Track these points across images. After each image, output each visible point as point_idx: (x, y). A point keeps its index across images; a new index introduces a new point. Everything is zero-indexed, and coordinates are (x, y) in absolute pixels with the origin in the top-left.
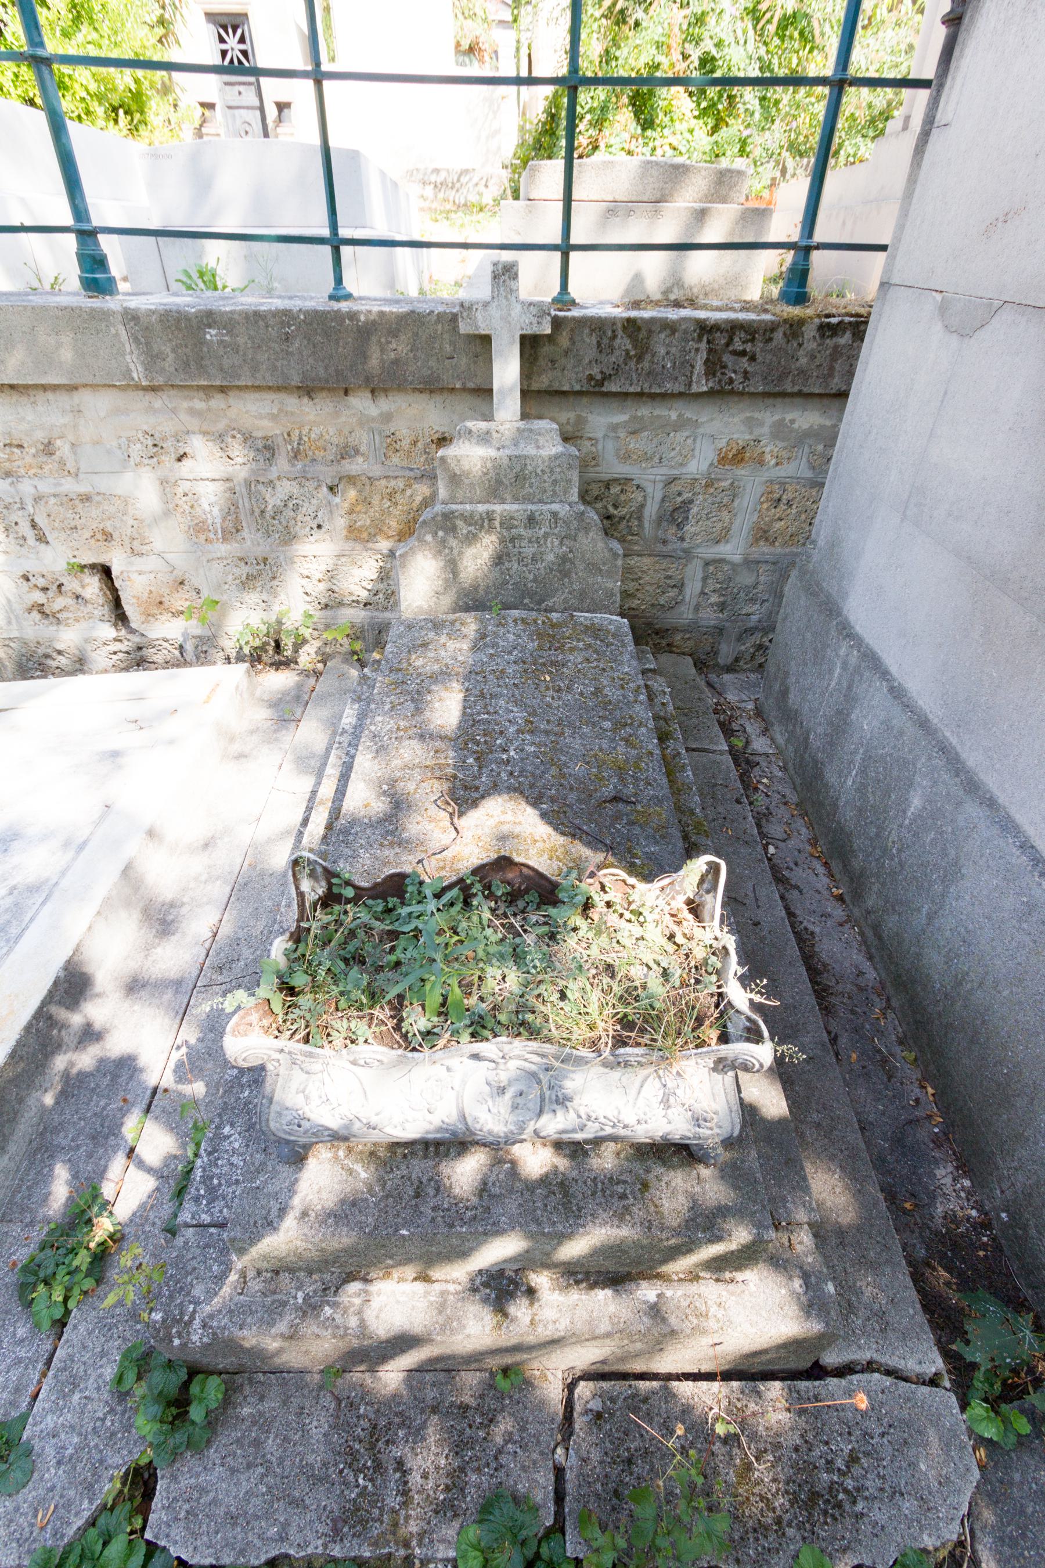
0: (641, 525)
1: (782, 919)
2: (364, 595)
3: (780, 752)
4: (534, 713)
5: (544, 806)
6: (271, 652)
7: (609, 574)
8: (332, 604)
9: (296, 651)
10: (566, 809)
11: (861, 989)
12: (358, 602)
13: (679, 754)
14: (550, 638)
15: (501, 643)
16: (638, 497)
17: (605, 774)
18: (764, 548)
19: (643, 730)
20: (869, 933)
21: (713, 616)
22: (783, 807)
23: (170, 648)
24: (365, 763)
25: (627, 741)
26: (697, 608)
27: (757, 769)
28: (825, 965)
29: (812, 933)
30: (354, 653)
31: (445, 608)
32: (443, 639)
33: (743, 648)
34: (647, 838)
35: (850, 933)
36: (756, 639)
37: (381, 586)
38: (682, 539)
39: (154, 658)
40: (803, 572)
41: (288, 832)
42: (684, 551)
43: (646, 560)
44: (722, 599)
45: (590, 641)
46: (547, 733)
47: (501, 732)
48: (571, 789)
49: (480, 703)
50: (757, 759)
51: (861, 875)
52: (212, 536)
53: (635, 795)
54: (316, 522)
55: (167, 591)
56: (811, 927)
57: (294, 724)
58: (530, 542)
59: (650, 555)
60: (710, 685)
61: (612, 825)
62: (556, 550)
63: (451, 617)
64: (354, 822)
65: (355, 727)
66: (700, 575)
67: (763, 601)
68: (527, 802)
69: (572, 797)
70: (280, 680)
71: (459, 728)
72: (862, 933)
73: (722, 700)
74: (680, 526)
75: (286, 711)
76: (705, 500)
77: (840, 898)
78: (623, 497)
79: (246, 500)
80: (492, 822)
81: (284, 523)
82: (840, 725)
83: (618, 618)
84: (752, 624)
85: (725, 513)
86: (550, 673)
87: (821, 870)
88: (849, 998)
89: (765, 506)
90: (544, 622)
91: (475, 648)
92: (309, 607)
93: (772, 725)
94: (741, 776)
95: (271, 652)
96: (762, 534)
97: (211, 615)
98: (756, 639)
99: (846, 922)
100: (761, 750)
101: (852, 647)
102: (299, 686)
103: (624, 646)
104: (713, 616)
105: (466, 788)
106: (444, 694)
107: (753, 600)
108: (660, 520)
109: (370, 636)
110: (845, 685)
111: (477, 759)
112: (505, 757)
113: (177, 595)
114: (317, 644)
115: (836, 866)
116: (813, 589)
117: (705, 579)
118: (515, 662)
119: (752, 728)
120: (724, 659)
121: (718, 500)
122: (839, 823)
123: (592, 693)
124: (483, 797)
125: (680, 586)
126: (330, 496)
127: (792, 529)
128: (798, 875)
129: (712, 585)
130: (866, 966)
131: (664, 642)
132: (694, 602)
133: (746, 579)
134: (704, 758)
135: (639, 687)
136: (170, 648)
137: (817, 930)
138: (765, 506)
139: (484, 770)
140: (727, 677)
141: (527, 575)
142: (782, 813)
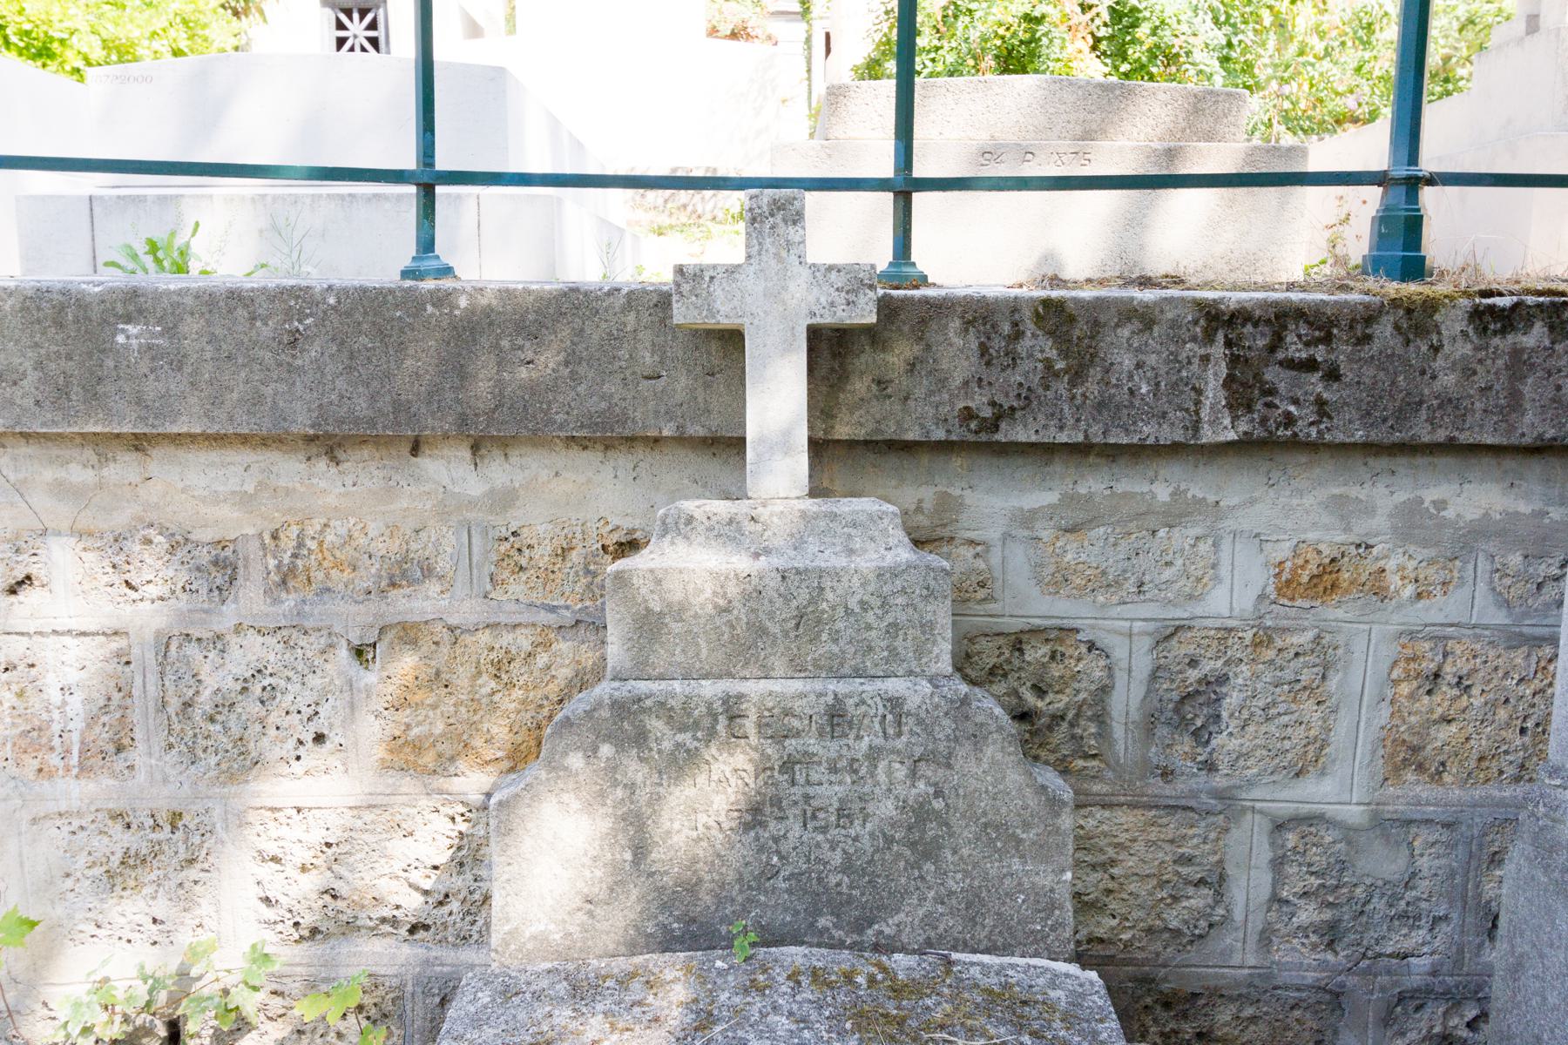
0: (1104, 734)
7: (1043, 852)
12: (394, 922)
16: (1094, 668)
18: (1414, 791)
21: (1310, 958)
26: (1266, 938)
37: (459, 882)
38: (1210, 766)
42: (1219, 795)
43: (1125, 817)
44: (1327, 915)
52: (54, 760)
54: (313, 727)
58: (833, 770)
59: (1133, 806)
62: (900, 790)
63: (622, 964)
66: (1264, 854)
67: (1437, 920)
74: (1200, 736)
76: (1257, 676)
78: (1056, 671)
79: (152, 678)
81: (236, 731)
83: (1073, 969)
84: (1415, 981)
85: (1310, 705)
89: (1405, 689)
90: (872, 980)
92: (270, 936)
96: (1407, 756)
107: (1409, 918)
108: (1150, 723)
117: (1278, 864)
121: (1288, 675)
125: (1216, 882)
126: (354, 668)
127: (1480, 744)
132: (1256, 923)
133: (1382, 863)
138: (1405, 689)
141: (826, 854)
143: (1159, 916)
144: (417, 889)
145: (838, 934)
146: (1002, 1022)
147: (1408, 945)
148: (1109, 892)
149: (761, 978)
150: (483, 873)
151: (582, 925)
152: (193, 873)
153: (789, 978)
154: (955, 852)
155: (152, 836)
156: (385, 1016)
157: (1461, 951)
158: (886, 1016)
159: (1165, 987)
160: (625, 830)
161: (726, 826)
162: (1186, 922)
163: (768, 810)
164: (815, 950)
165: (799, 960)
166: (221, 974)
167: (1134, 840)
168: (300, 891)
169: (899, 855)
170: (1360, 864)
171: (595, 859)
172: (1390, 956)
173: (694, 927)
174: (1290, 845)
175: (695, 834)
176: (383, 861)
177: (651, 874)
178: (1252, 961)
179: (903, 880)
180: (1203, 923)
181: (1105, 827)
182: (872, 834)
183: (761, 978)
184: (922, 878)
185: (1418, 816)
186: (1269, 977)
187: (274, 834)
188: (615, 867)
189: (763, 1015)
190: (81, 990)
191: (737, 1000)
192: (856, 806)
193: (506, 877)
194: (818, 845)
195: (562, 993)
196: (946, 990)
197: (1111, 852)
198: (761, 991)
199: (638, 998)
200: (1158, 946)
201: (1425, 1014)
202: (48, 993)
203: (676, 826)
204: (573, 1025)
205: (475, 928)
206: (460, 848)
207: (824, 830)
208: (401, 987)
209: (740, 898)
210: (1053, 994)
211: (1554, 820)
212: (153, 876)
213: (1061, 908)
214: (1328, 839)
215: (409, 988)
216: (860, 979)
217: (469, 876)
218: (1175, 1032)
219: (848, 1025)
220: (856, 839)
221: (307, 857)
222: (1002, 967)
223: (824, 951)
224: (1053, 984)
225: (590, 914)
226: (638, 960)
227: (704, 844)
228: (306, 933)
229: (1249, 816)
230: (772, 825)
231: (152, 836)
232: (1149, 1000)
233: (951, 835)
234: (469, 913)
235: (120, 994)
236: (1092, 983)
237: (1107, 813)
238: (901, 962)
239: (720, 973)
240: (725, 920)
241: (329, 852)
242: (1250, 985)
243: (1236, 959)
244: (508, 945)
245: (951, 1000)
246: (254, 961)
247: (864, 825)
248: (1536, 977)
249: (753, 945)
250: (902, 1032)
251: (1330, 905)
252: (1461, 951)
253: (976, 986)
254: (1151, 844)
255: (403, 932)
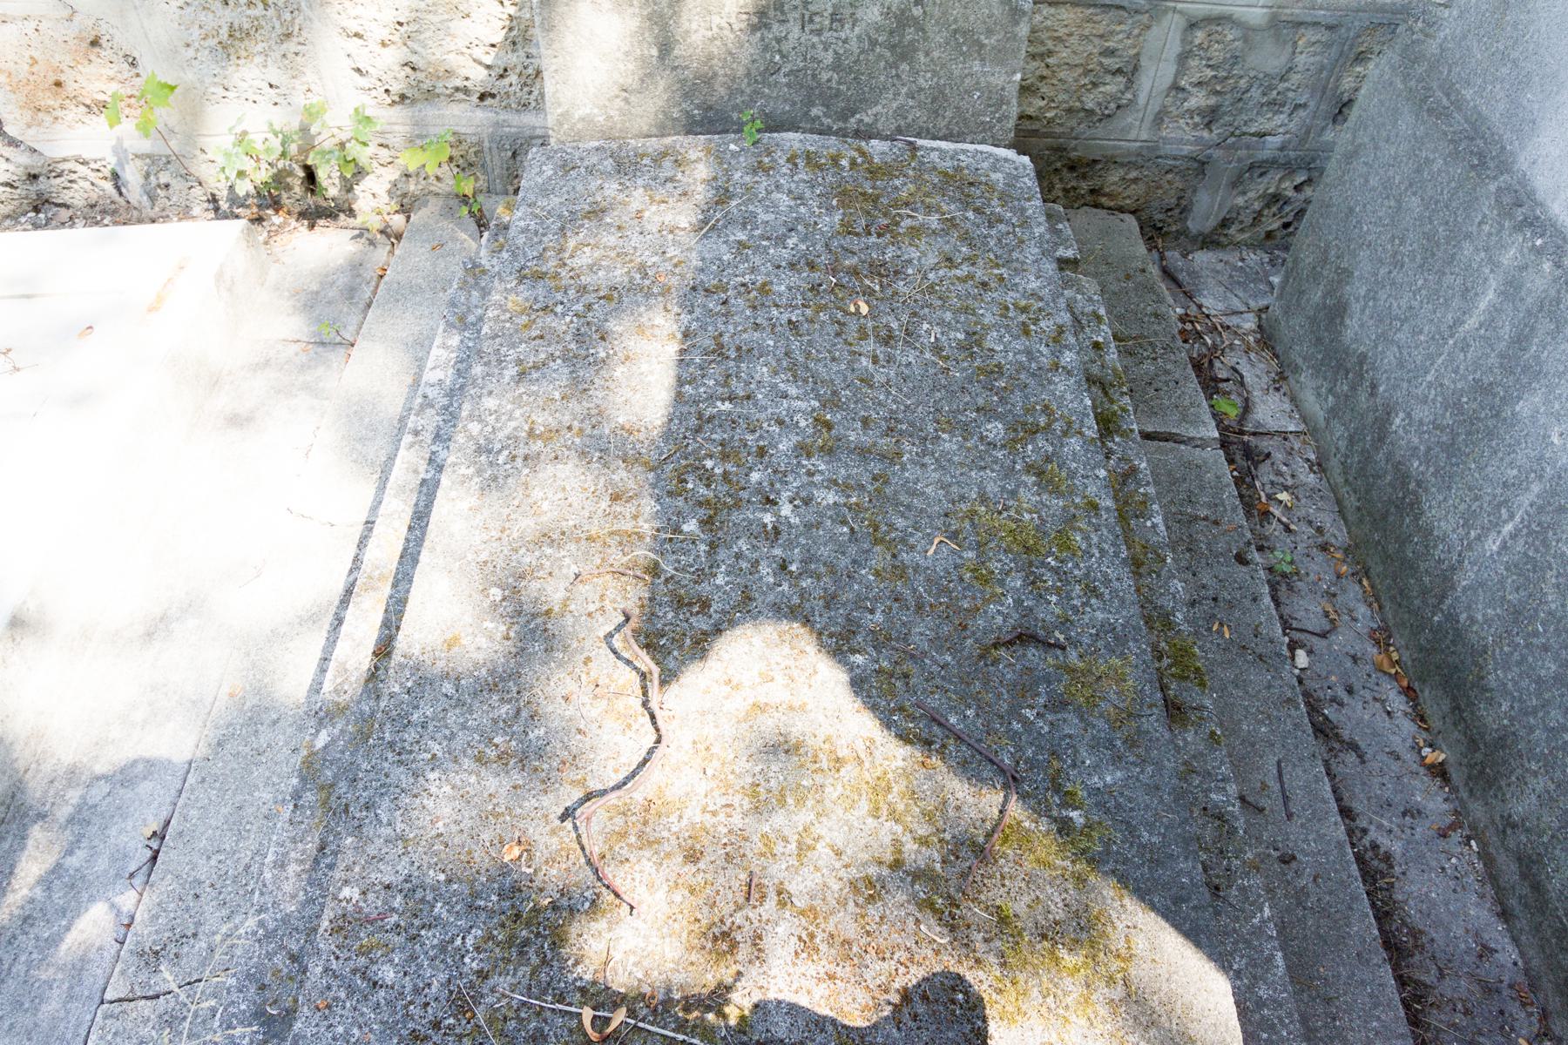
1: (1340, 844)
2: (478, 77)
3: (1311, 431)
4: (832, 402)
5: (859, 659)
6: (300, 191)
7: (1000, 56)
8: (419, 90)
9: (350, 190)
10: (908, 666)
11: (1489, 990)
12: (466, 91)
13: (1134, 470)
14: (867, 202)
15: (762, 217)
17: (995, 566)
19: (1074, 443)
20: (1509, 870)
21: (1190, 135)
22: (1320, 557)
23: (92, 176)
24: (456, 508)
25: (1040, 473)
26: (1159, 119)
27: (1265, 468)
28: (1415, 934)
29: (1387, 858)
30: (464, 199)
31: (643, 124)
32: (638, 199)
33: (1240, 201)
34: (1094, 746)
35: (1463, 856)
36: (1271, 182)
37: (513, 59)
39: (65, 197)
40: (1411, 57)
41: (313, 619)
44: (1212, 101)
45: (952, 209)
46: (863, 452)
47: (762, 452)
48: (919, 607)
49: (714, 370)
50: (1265, 444)
51: (1502, 742)
53: (1065, 623)
55: (68, 60)
56: (1385, 842)
57: (342, 350)
60: (1168, 274)
61: (1014, 712)
63: (654, 144)
64: (423, 682)
65: (450, 394)
66: (1174, 48)
67: (1297, 107)
68: (821, 645)
69: (921, 631)
70: (326, 247)
71: (667, 435)
72: (1486, 856)
73: (1193, 310)
75: (337, 312)
77: (1439, 772)
80: (739, 704)
82: (1479, 417)
83: (1011, 154)
84: (1265, 154)
86: (868, 293)
87: (1398, 703)
88: (1467, 1012)
90: (853, 163)
91: (706, 226)
92: (366, 99)
93: (1296, 369)
94: (1238, 482)
95: (300, 191)
97: (166, 114)
98: (1271, 182)
99: (1453, 827)
100: (1272, 425)
101: (1539, 251)
102: (356, 267)
103: (1025, 223)
104: (1190, 135)
105: (679, 603)
106: (634, 344)
107: (1275, 105)
109: (496, 162)
110: (1506, 331)
111: (706, 523)
112: (768, 519)
113: (87, 69)
114: (392, 174)
115: (1435, 703)
116: (1435, 98)
117: (1183, 58)
118: (792, 266)
119: (1255, 372)
120: (1202, 218)
122: (1451, 617)
123: (961, 347)
124: (718, 631)
125: (1130, 72)
128: (1353, 717)
129: (1198, 70)
130: (1496, 933)
131: (1084, 186)
132: (1155, 107)
133: (1268, 59)
134: (1172, 455)
135: (1060, 330)
136: (92, 176)
137: (1396, 848)
139: (722, 554)
140: (1202, 258)
141: (821, 54)
142: (1318, 569)
143: (1079, 99)
144: (480, 63)
145: (827, 121)
146: (953, 200)
147: (1268, 126)
148: (1042, 78)
149: (766, 160)
150: (533, 51)
151: (620, 109)
152: (291, 46)
153: (788, 160)
154: (927, 54)
155: (249, 12)
156: (471, 165)
157: (1308, 132)
158: (863, 194)
159: (1073, 155)
160: (651, 29)
161: (736, 27)
162: (1099, 104)
163: (771, 13)
164: (808, 136)
165: (797, 145)
166: (336, 131)
167: (1071, 35)
168: (387, 62)
169: (880, 56)
170: (1249, 60)
171: (627, 54)
172: (1253, 135)
173: (711, 114)
174: (1197, 42)
175: (709, 34)
176: (448, 39)
177: (675, 68)
178: (1144, 136)
179: (882, 78)
180: (1113, 105)
181: (1049, 23)
182: (859, 37)
183: (766, 160)
184: (898, 76)
185: (1309, 19)
186: (1156, 148)
187: (353, 13)
188: (643, 60)
189: (769, 193)
190: (227, 141)
191: (748, 179)
192: (847, 12)
193: (554, 67)
194: (813, 46)
195: (609, 169)
196: (911, 173)
197: (1050, 44)
198: (766, 171)
199: (669, 174)
200: (1073, 123)
201: (1265, 179)
202: (204, 142)
203: (694, 26)
204: (621, 197)
205: (532, 97)
206: (511, 29)
207: (819, 32)
208: (480, 143)
209: (748, 91)
210: (994, 176)
211: (1426, 35)
212: (260, 47)
213: (1008, 103)
214: (1230, 37)
215: (486, 144)
216: (844, 162)
217: (522, 53)
218: (1074, 188)
219: (834, 202)
220: (845, 41)
221: (385, 34)
222: (956, 152)
223: (816, 137)
224: (994, 169)
225: (626, 100)
226: (668, 140)
227: (718, 43)
228: (397, 99)
229: (1170, 15)
230: (775, 26)
231: (249, 12)
232: (1059, 165)
233: (925, 40)
234: (525, 84)
235: (259, 146)
236: (1025, 168)
237: (1052, 10)
238: (877, 147)
239: (734, 155)
240: (735, 108)
241: (402, 29)
242: (1139, 155)
243: (1132, 136)
244: (561, 124)
245: (915, 180)
246: (360, 122)
247: (852, 29)
248: (1366, 164)
249: (759, 131)
250: (876, 208)
251: (1217, 93)
252: (1308, 132)
253: (935, 168)
254: (1084, 38)
255: (475, 98)
